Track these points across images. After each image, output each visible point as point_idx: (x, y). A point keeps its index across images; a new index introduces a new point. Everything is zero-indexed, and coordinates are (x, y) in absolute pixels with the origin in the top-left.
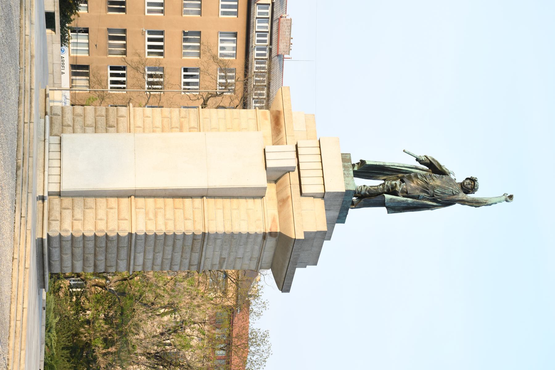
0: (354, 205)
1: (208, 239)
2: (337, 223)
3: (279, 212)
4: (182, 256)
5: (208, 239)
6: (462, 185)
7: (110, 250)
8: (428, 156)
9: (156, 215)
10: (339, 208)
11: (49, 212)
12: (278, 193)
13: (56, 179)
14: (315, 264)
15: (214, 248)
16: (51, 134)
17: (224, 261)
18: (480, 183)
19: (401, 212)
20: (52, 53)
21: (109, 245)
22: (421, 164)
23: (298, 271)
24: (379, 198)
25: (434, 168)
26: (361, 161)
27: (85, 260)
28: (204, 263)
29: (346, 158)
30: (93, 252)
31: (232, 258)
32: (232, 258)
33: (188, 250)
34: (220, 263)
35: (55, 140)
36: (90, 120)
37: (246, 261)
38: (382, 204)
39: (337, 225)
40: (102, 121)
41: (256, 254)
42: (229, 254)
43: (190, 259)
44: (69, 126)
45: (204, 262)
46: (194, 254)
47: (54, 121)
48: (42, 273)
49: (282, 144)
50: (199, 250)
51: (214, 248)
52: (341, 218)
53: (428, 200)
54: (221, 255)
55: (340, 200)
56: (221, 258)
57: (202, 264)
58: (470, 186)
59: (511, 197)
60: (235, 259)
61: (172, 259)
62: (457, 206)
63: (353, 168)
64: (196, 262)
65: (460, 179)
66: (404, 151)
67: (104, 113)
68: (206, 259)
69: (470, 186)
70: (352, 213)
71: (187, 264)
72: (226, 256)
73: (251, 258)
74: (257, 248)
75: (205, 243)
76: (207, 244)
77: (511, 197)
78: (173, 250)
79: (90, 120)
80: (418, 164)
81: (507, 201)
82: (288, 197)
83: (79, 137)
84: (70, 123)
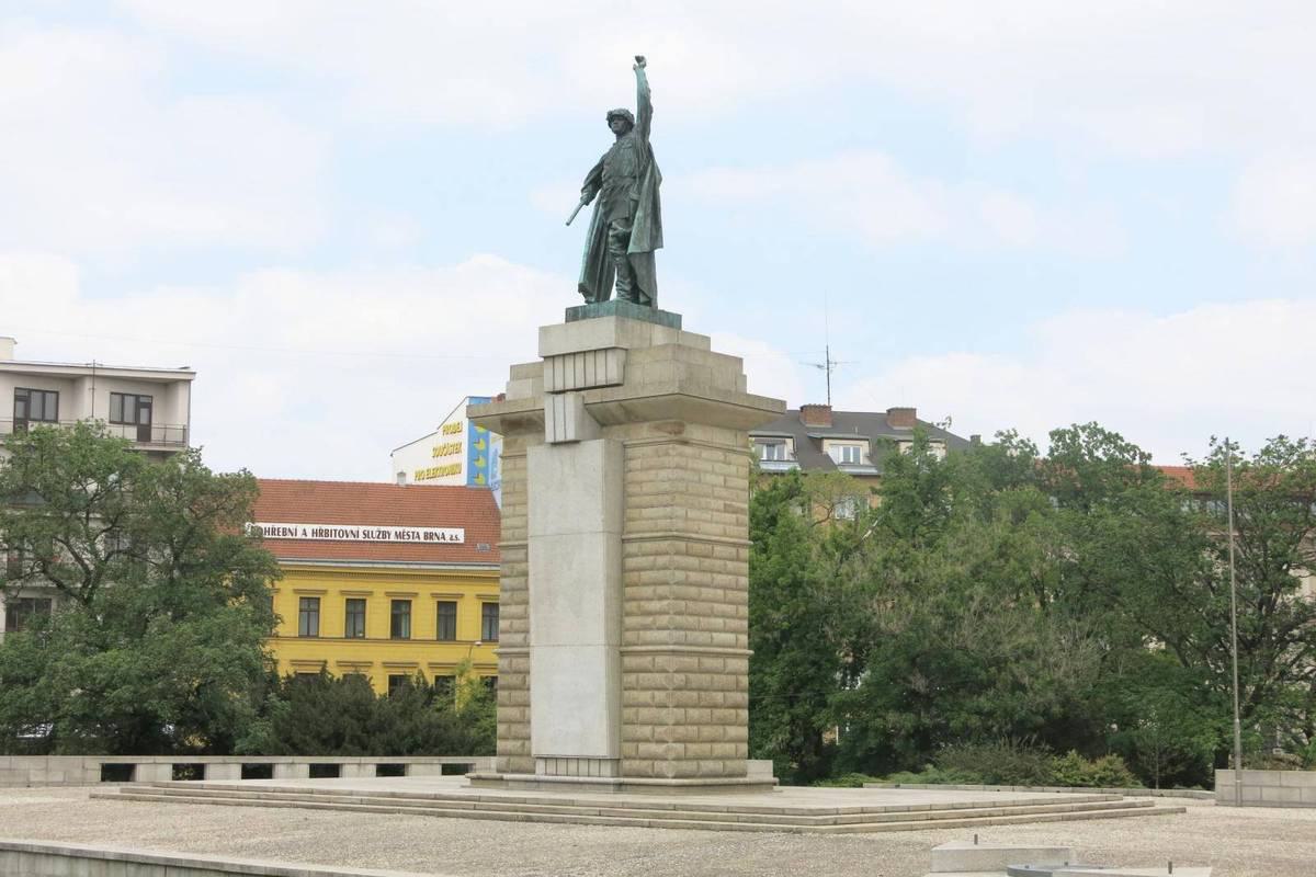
0: (650, 302)
1: (687, 531)
2: (680, 328)
3: (645, 419)
4: (720, 573)
5: (687, 531)
6: (619, 134)
7: (705, 685)
8: (582, 186)
9: (649, 613)
10: (646, 326)
11: (642, 777)
12: (620, 423)
13: (594, 767)
14: (741, 360)
15: (705, 521)
16: (534, 772)
17: (730, 506)
18: (615, 107)
19: (660, 227)
20: (1162, 795)
21: (694, 685)
22: (593, 198)
23: (751, 389)
24: (636, 263)
25: (595, 182)
26: (580, 291)
27: (724, 723)
28: (736, 537)
29: (573, 315)
30: (708, 711)
31: (724, 493)
32: (724, 493)
33: (707, 563)
34: (734, 512)
35: (540, 765)
36: (513, 713)
37: (733, 469)
38: (649, 255)
39: (684, 328)
40: (517, 695)
41: (719, 455)
42: (720, 498)
43: (724, 559)
44: (523, 745)
45: (731, 537)
46: (716, 554)
47: (517, 767)
48: (743, 787)
49: (544, 414)
50: (707, 546)
51: (705, 521)
52: (673, 321)
53: (641, 183)
54: (718, 511)
55: (630, 323)
56: (725, 511)
57: (736, 540)
58: (619, 121)
59: (639, 59)
60: (725, 486)
61: (725, 588)
62: (652, 139)
63: (591, 303)
64: (734, 550)
65: (610, 139)
66: (568, 224)
67: (506, 693)
68: (725, 535)
69: (619, 121)
70: (664, 303)
71: (735, 564)
72: (721, 503)
73: (724, 462)
74: (705, 454)
75: (694, 536)
76: (697, 533)
77: (639, 59)
78: (707, 586)
79: (513, 713)
80: (593, 203)
81: (644, 66)
82: (622, 406)
83: (536, 730)
84: (519, 743)
